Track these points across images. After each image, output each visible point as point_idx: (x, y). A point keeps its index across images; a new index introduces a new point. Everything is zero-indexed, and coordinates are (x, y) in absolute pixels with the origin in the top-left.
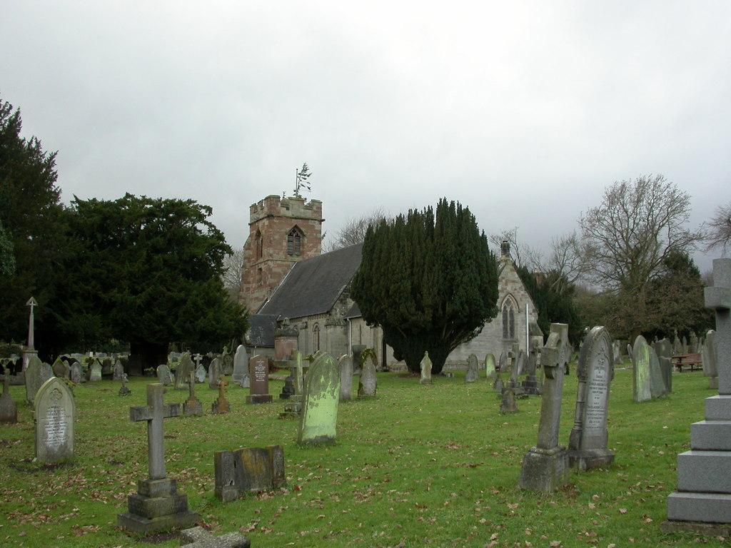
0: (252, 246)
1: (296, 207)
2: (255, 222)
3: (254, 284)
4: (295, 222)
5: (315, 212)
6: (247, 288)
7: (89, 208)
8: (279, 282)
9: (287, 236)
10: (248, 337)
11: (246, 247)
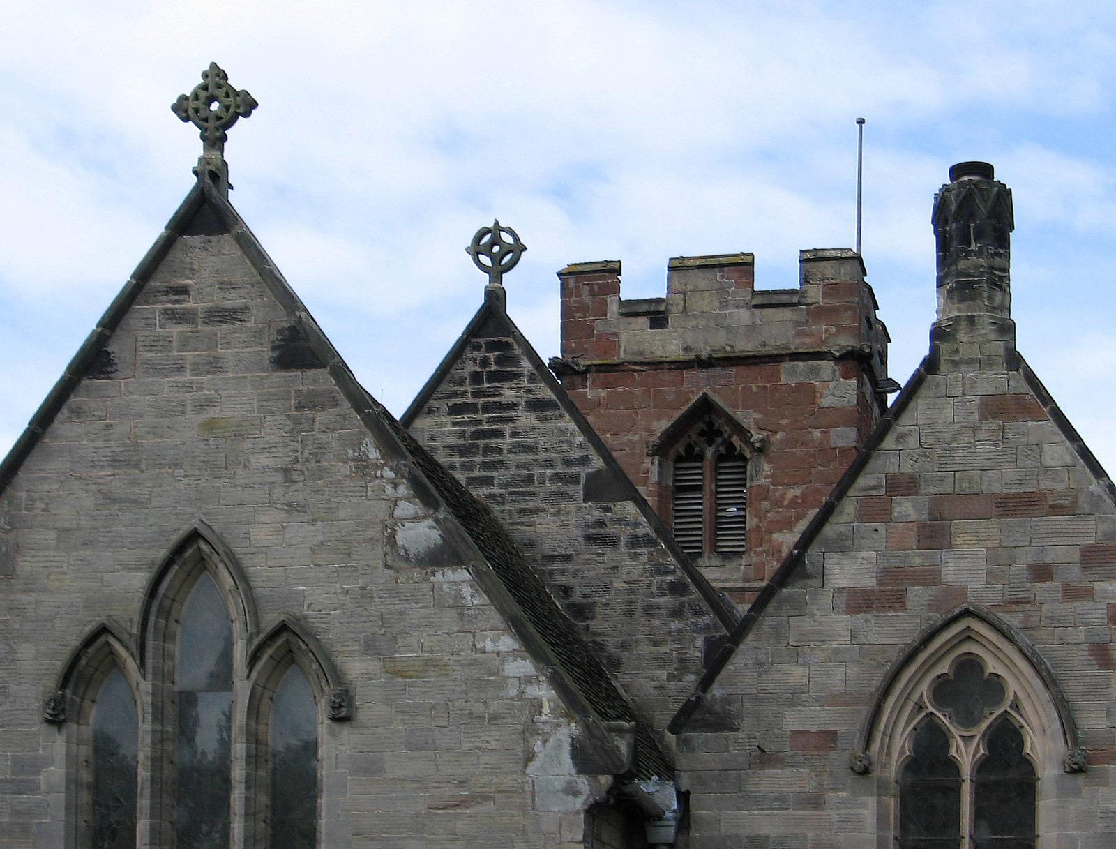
4: (696, 386)
7: (930, 351)
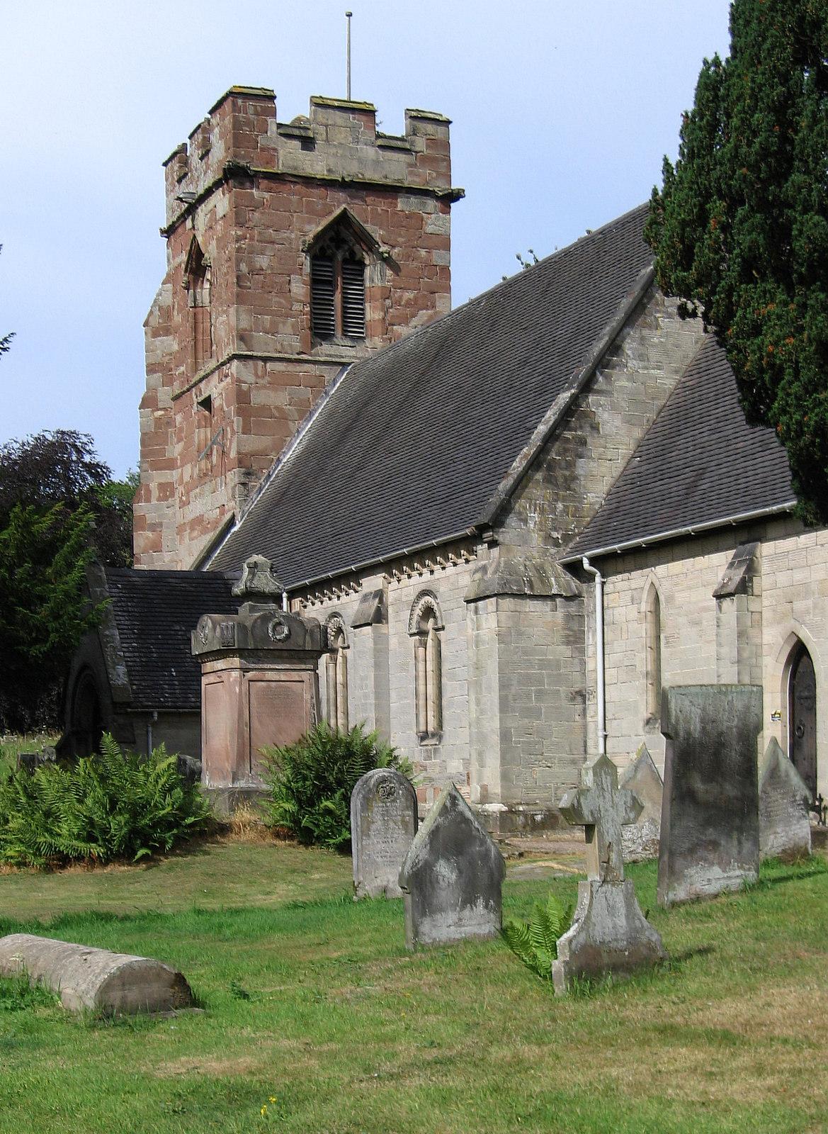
0: (177, 318)
1: (341, 136)
2: (182, 218)
3: (188, 468)
4: (339, 204)
5: (426, 160)
6: (162, 487)
8: (280, 447)
9: (306, 261)
10: (122, 669)
11: (155, 321)
